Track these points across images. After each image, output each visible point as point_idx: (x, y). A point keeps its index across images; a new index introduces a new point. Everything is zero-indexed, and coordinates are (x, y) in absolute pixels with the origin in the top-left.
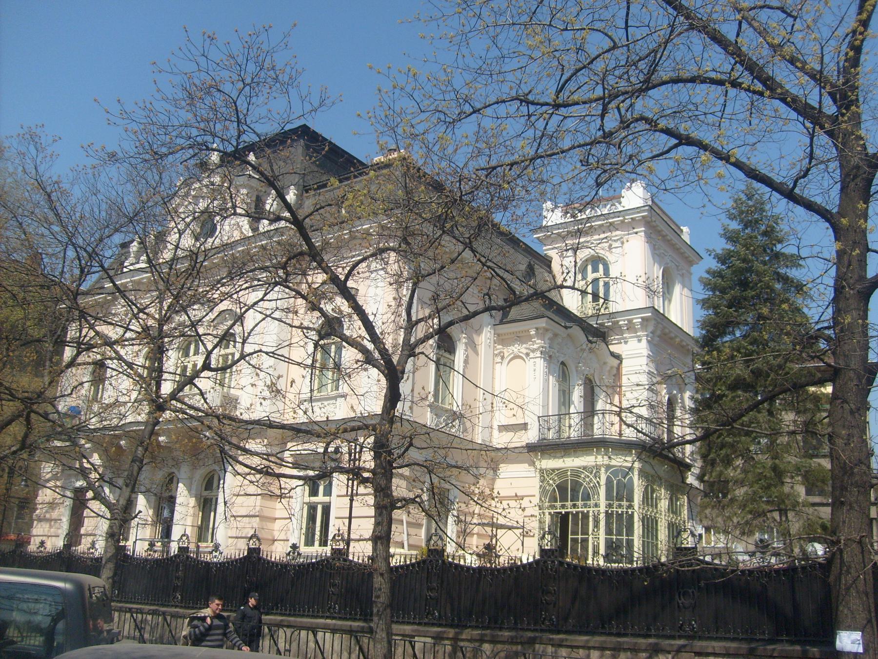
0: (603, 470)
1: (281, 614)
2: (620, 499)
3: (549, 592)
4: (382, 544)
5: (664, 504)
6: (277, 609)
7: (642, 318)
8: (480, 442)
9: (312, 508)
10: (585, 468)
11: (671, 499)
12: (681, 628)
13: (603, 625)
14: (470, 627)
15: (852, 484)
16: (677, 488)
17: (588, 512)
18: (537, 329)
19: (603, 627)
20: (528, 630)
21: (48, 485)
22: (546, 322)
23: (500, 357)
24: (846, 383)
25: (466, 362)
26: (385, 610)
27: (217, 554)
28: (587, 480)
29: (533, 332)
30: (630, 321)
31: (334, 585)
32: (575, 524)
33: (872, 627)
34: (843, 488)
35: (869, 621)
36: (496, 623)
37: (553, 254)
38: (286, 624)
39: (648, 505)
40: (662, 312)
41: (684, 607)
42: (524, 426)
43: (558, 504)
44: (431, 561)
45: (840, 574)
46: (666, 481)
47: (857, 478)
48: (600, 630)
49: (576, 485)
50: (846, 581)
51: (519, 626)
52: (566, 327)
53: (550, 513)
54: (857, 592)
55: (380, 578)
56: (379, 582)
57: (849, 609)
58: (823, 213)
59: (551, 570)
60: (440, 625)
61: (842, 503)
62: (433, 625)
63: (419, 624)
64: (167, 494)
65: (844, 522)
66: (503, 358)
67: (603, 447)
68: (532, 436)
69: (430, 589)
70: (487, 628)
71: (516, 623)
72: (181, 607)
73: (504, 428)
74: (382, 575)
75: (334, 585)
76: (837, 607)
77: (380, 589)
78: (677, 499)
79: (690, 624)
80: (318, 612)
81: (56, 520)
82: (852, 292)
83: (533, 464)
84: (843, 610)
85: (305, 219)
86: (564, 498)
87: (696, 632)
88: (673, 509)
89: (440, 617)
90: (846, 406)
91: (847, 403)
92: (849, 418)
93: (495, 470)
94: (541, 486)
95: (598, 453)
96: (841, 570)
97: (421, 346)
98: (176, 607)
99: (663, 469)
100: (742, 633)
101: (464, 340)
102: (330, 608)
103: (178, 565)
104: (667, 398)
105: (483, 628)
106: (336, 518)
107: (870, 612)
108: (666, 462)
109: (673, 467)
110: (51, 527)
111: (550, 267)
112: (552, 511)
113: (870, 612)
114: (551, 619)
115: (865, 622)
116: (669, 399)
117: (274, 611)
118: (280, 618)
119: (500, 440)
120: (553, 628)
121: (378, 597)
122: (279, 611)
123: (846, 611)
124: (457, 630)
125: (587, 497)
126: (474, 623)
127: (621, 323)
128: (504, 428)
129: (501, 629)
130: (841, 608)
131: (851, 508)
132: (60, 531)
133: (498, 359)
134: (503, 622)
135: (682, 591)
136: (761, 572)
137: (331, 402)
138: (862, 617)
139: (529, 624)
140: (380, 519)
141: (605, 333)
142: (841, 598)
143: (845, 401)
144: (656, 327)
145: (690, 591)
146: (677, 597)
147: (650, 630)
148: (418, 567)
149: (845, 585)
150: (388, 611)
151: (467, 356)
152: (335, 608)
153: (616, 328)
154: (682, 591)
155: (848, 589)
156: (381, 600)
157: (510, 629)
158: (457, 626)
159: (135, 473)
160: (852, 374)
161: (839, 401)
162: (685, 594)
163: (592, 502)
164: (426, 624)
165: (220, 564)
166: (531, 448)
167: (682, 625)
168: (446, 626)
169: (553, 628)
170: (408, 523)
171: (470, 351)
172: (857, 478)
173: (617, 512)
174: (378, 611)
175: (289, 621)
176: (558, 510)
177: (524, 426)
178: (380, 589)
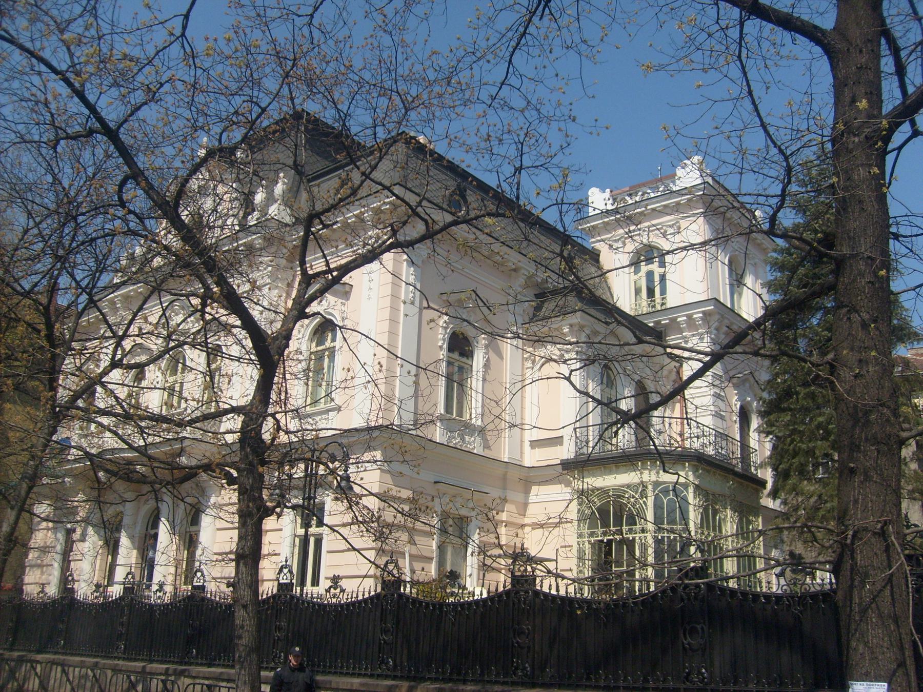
0: (650, 487)
1: (224, 666)
2: (672, 522)
3: (521, 633)
4: (245, 564)
5: (730, 527)
6: (220, 660)
7: (703, 312)
8: (506, 460)
9: (305, 541)
10: (628, 486)
11: (741, 520)
12: (687, 678)
13: (588, 674)
14: (429, 679)
15: (867, 440)
16: (747, 509)
17: (634, 539)
18: (571, 326)
19: (588, 679)
20: (497, 682)
21: (41, 527)
22: (582, 317)
23: (530, 362)
24: (854, 280)
25: (487, 366)
26: (248, 655)
27: (161, 594)
28: (632, 500)
29: (566, 330)
30: (689, 317)
31: (279, 629)
32: (620, 551)
33: (907, 674)
34: (854, 447)
35: (902, 664)
36: (459, 674)
37: (602, 248)
38: (225, 677)
39: (708, 528)
40: (729, 306)
41: (691, 649)
42: (557, 441)
43: (600, 531)
44: (385, 596)
45: (852, 587)
46: (732, 501)
47: (875, 429)
48: (584, 682)
49: (620, 509)
50: (861, 598)
51: (486, 678)
52: (607, 323)
53: (589, 542)
54: (880, 616)
55: (242, 612)
56: (241, 616)
57: (866, 644)
58: (812, 33)
59: (524, 604)
60: (395, 678)
61: (852, 471)
62: (387, 677)
63: (372, 676)
64: (152, 532)
65: (856, 501)
66: (534, 362)
67: (649, 460)
68: (567, 451)
69: (385, 631)
70: (450, 680)
71: (482, 674)
72: (124, 659)
73: (535, 444)
74: (245, 607)
75: (279, 629)
76: (848, 641)
77: (242, 627)
78: (749, 522)
79: (700, 673)
80: (342, 667)
81: (47, 565)
82: (856, 140)
83: (568, 484)
84: (858, 648)
85: (119, 128)
86: (605, 524)
87: (706, 684)
88: (743, 533)
89: (395, 665)
90: (855, 317)
91: (857, 312)
92: (861, 335)
93: (527, 492)
94: (579, 510)
95: (644, 468)
96: (853, 580)
97: (315, 304)
98: (119, 659)
99: (727, 486)
100: (769, 684)
101: (483, 342)
102: (517, 668)
103: (123, 610)
104: (738, 406)
105: (445, 680)
106: (329, 552)
107: (902, 649)
108: (731, 476)
109: (741, 484)
110: (42, 573)
111: (598, 261)
112: (592, 540)
113: (902, 649)
114: (525, 668)
115: (894, 666)
116: (742, 408)
117: (217, 662)
118: (219, 670)
119: (532, 458)
120: (526, 680)
121: (240, 637)
122: (221, 662)
123: (861, 647)
124: (413, 683)
125: (632, 521)
126: (433, 675)
127: (679, 320)
128: (535, 444)
129: (465, 682)
130: (853, 644)
131: (867, 477)
132: (51, 578)
133: (529, 364)
134: (466, 674)
135: (688, 628)
136: (793, 598)
137: (323, 417)
138: (888, 658)
139: (498, 675)
140: (244, 530)
141: (661, 332)
142: (853, 626)
143: (854, 309)
144: (720, 321)
145: (699, 627)
146: (682, 635)
147: (648, 681)
148: (372, 603)
149: (860, 604)
150: (254, 657)
151: (488, 360)
152: (280, 656)
153: (673, 325)
154: (688, 628)
155: (864, 611)
156: (244, 641)
157: (475, 682)
158: (414, 679)
159: (23, 493)
160: (862, 266)
161: (845, 310)
162: (693, 631)
163: (638, 527)
164: (379, 676)
165: (164, 606)
166: (567, 466)
167: (689, 674)
168: (402, 678)
169: (526, 680)
170: (410, 556)
171: (492, 354)
172: (875, 429)
173: (669, 537)
174: (240, 657)
175: (229, 674)
176: (600, 538)
177: (557, 441)
178: (242, 627)
